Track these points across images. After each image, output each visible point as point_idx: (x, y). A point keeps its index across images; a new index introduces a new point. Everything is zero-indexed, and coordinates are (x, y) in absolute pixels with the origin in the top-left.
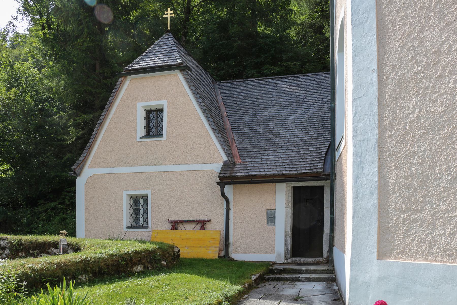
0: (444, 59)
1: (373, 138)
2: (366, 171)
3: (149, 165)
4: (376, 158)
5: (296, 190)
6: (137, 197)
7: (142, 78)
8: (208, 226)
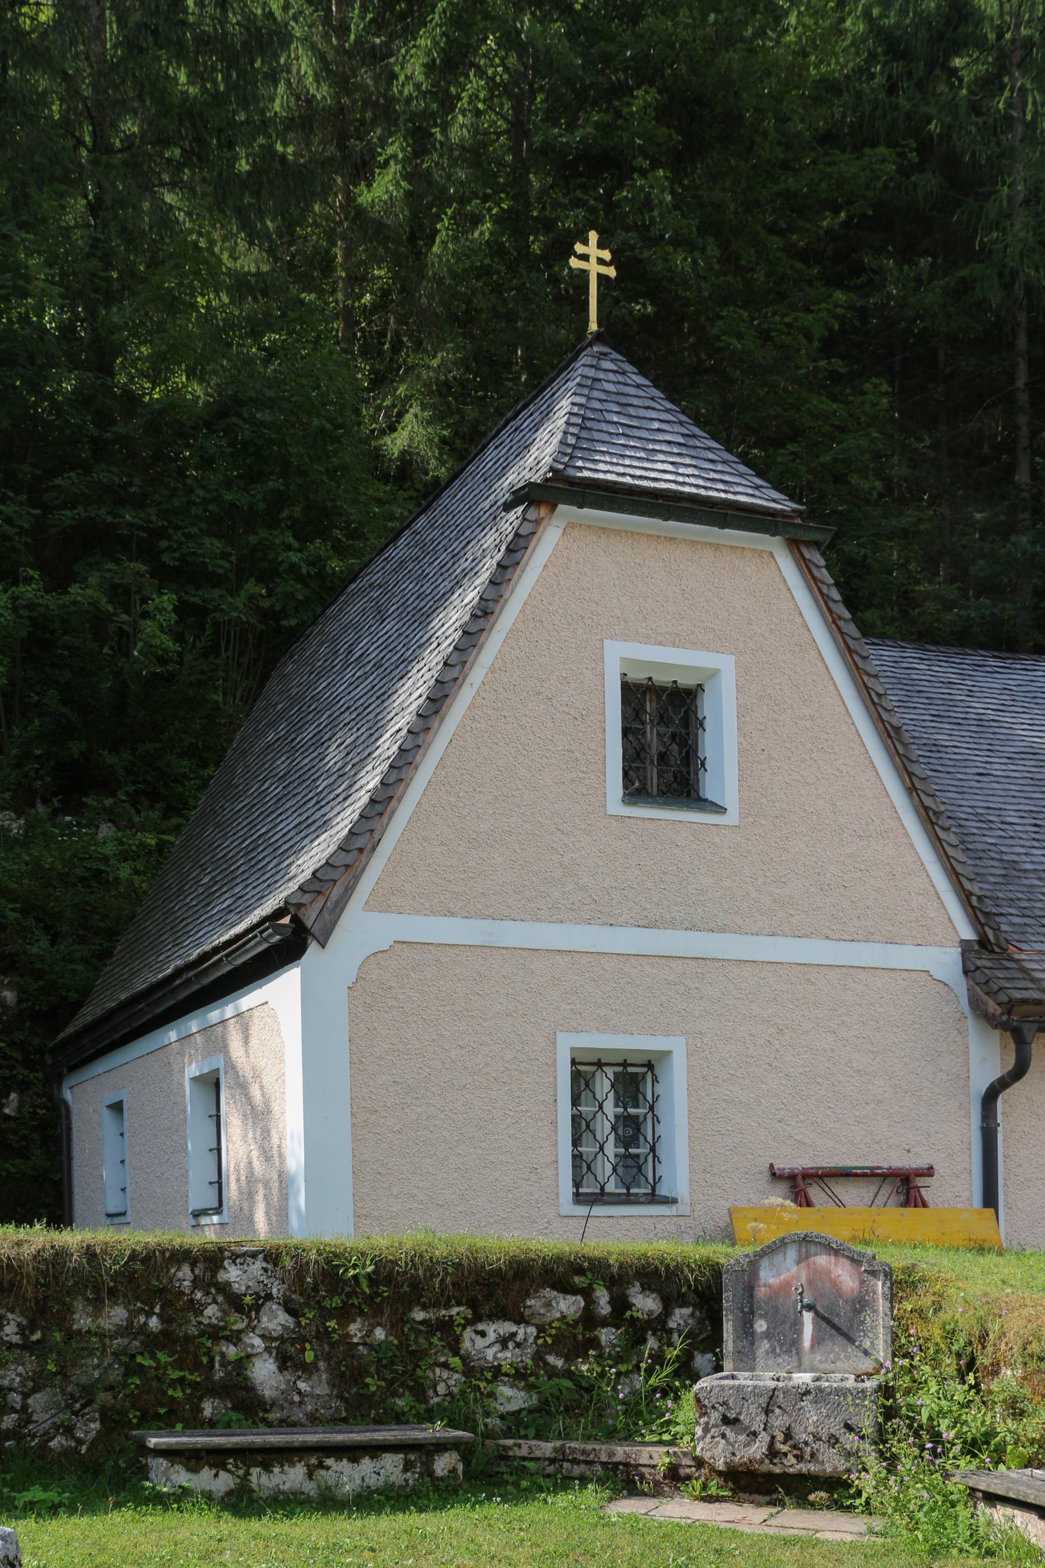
3: (672, 924)
6: (625, 1064)
7: (617, 532)
8: (931, 1190)
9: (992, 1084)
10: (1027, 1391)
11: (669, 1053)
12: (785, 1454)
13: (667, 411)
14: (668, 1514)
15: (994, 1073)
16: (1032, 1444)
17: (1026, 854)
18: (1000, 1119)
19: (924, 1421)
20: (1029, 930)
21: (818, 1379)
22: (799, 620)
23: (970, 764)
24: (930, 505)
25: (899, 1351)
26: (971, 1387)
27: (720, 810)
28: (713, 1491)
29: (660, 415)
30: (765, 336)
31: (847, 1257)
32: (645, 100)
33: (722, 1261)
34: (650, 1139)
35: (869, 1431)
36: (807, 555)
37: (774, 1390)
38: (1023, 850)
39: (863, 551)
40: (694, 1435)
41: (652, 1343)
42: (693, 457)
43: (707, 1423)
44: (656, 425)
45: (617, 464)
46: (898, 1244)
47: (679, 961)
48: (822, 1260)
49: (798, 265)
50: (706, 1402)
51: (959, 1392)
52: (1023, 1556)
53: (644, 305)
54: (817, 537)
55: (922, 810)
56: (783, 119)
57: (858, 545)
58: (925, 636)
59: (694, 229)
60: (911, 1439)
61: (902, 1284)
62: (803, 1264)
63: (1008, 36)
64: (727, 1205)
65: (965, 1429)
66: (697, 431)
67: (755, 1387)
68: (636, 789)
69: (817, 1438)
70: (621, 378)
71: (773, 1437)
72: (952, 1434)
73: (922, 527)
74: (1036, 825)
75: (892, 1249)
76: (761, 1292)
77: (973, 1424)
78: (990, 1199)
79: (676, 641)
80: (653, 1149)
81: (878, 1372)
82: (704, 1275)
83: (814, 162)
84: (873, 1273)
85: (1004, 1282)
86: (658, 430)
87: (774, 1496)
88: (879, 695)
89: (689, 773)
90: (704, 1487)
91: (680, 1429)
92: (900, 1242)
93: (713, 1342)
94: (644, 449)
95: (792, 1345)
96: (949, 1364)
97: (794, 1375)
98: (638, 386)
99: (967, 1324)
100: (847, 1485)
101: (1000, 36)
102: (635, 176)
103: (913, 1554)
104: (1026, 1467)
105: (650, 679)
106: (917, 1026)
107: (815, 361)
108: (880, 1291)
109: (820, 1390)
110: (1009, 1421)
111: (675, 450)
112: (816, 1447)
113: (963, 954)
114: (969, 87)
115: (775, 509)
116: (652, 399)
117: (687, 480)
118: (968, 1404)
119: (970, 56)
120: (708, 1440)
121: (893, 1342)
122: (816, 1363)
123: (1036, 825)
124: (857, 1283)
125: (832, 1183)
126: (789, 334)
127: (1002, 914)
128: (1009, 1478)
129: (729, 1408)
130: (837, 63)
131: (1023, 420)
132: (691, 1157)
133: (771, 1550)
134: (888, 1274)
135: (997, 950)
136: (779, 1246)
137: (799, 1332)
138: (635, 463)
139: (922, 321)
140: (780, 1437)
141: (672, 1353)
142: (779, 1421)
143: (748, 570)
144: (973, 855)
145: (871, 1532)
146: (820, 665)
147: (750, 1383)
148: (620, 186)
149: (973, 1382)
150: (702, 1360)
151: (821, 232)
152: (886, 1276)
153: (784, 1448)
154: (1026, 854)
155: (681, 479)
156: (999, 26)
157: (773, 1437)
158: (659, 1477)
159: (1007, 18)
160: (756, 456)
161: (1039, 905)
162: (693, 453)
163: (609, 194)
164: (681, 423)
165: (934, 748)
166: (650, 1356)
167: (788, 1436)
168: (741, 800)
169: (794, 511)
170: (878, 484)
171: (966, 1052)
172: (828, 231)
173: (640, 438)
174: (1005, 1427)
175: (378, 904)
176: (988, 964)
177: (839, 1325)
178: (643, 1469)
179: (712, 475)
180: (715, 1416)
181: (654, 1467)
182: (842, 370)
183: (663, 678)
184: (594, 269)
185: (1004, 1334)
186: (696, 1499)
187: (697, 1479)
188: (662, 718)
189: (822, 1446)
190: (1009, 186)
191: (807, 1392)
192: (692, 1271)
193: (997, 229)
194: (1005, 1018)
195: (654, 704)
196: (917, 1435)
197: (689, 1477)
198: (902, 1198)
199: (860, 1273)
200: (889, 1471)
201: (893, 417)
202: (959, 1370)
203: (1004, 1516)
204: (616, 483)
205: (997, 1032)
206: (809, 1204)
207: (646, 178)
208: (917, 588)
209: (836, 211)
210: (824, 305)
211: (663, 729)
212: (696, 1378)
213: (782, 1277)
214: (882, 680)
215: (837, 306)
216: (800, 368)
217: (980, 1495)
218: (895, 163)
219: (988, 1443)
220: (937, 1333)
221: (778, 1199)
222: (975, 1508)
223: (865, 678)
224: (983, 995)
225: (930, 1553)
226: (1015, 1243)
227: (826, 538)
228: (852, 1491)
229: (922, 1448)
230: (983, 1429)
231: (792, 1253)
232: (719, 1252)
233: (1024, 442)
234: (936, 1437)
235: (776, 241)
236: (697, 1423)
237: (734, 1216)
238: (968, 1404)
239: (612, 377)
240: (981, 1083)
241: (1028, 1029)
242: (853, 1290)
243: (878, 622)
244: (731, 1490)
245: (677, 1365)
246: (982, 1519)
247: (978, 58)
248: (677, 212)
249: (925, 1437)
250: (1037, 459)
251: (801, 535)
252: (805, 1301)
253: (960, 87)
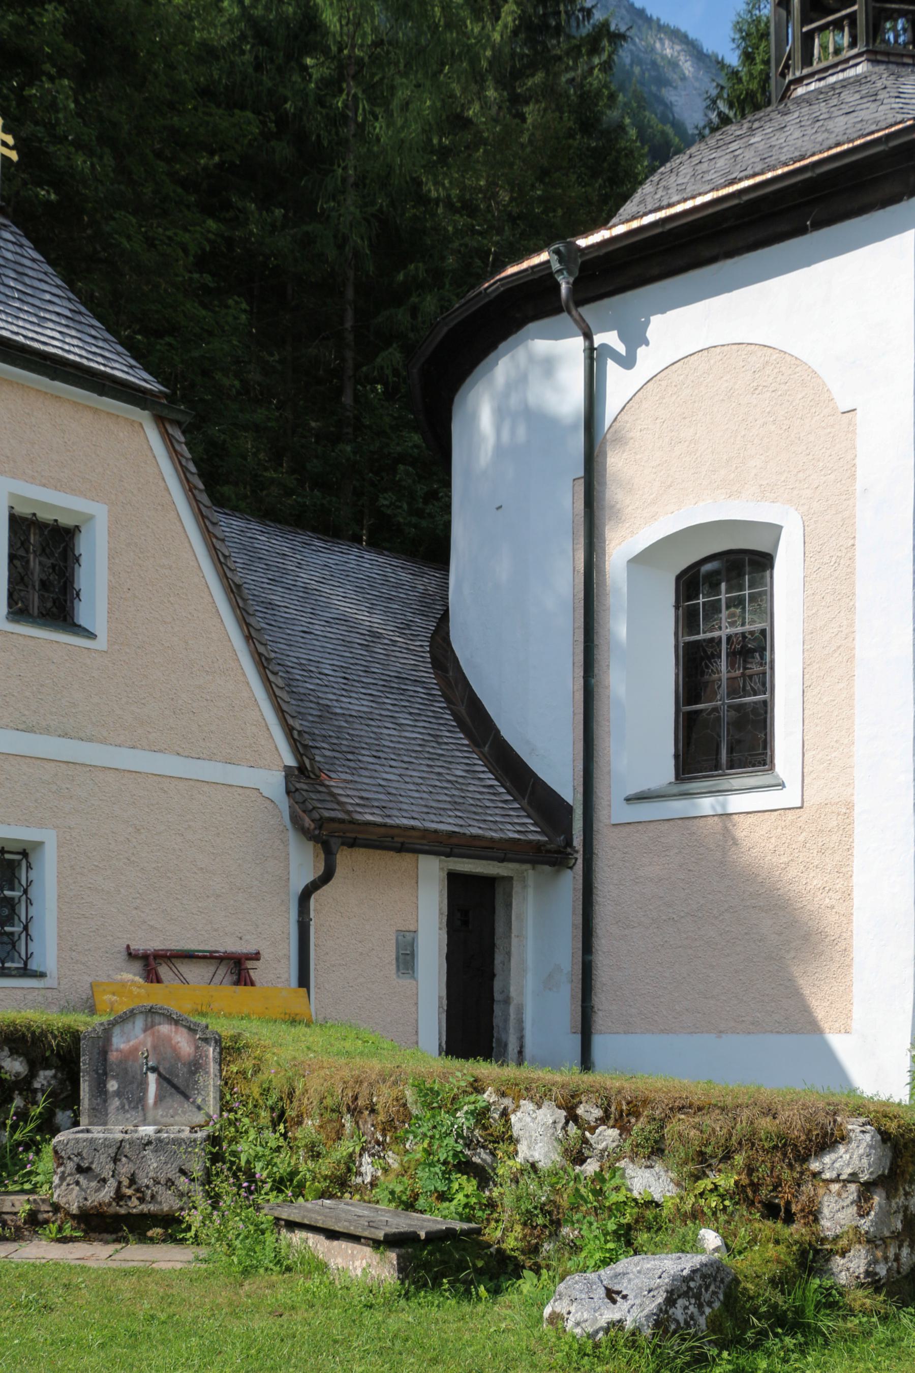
3: (47, 731)
7: (10, 383)
9: (307, 886)
10: (322, 1137)
11: (41, 844)
12: (130, 1197)
13: (58, 286)
14: (26, 1256)
15: (309, 877)
16: (325, 1180)
17: (337, 701)
18: (312, 915)
19: (243, 1163)
20: (337, 762)
21: (159, 1131)
22: (161, 483)
23: (297, 622)
24: (278, 409)
25: (225, 1106)
26: (281, 1135)
27: (91, 636)
28: (67, 1232)
29: (50, 287)
30: (151, 243)
31: (185, 1026)
32: (54, 15)
33: (82, 1028)
34: (23, 919)
35: (198, 1173)
36: (170, 431)
37: (121, 1141)
38: (334, 697)
39: (223, 437)
40: (51, 1183)
41: (18, 1102)
42: (78, 331)
43: (63, 1173)
44: (48, 297)
45: (12, 324)
46: (228, 1016)
47: (53, 764)
48: (165, 1029)
49: (179, 190)
50: (63, 1154)
51: (273, 1139)
52: (313, 1269)
53: (48, 192)
54: (179, 417)
55: (256, 656)
56: (171, 67)
57: (219, 430)
58: (269, 514)
59: (94, 138)
60: (231, 1180)
61: (229, 1050)
62: (148, 1032)
63: (346, 52)
64: (90, 979)
65: (275, 1169)
66: (83, 309)
67: (105, 1139)
68: (19, 610)
69: (157, 1182)
70: (18, 250)
71: (120, 1183)
72: (265, 1174)
73: (269, 424)
74: (345, 678)
75: (223, 1021)
76: (113, 1056)
77: (280, 1166)
78: (304, 980)
79: (58, 485)
80: (26, 928)
81: (207, 1125)
82: (65, 1040)
83: (195, 109)
84: (206, 1040)
85: (309, 1048)
86: (50, 302)
87: (120, 1234)
88: (225, 557)
89: (66, 601)
90: (60, 1229)
91: (40, 1178)
92: (230, 1014)
93: (71, 1100)
94: (36, 315)
95: (139, 1102)
96: (265, 1116)
97: (140, 1128)
98: (34, 260)
99: (279, 1082)
100: (179, 1221)
101: (340, 50)
102: (44, 79)
103: (229, 1275)
104: (320, 1198)
105: (34, 514)
106: (249, 834)
107: (190, 272)
108: (211, 1055)
109: (160, 1140)
110: (309, 1162)
111: (63, 322)
112: (155, 1189)
113: (286, 777)
114: (316, 83)
115: (145, 388)
116: (45, 273)
117: (72, 349)
118: (278, 1149)
119: (318, 59)
120: (64, 1187)
121: (221, 1099)
122: (158, 1117)
123: (345, 678)
124: (193, 1049)
125: (174, 960)
126: (170, 245)
127: (317, 748)
128: (308, 1208)
129: (83, 1159)
130: (216, 33)
131: (349, 354)
132: (59, 937)
133: (113, 1281)
134: (218, 1042)
135: (313, 776)
136: (129, 1016)
137: (145, 1090)
138: (28, 326)
139: (275, 259)
140: (126, 1182)
141: (36, 1111)
142: (125, 1168)
143: (121, 434)
144: (297, 697)
145: (197, 1259)
146: (178, 524)
147: (101, 1135)
148: (31, 85)
149: (283, 1131)
150: (62, 1117)
151: (199, 168)
152: (216, 1043)
153: (129, 1192)
154: (337, 701)
155: (67, 347)
156: (339, 43)
157: (120, 1183)
158: (20, 1223)
159: (345, 38)
160: (139, 341)
161: (345, 742)
162: (78, 327)
163: (21, 87)
164: (69, 299)
165: (269, 606)
166: (15, 1114)
167: (133, 1181)
168: (109, 629)
169: (161, 392)
170: (237, 383)
171: (287, 858)
172: (205, 168)
173: (33, 305)
174: (305, 1167)
176: (305, 787)
177: (178, 1084)
178: (6, 1217)
179: (94, 349)
180: (70, 1166)
181: (15, 1214)
182: (212, 285)
183: (45, 516)
185: (307, 1091)
186: (53, 1240)
187: (53, 1223)
188: (43, 550)
189: (159, 1189)
190: (343, 169)
191: (149, 1143)
192: (55, 1037)
193: (334, 200)
194: (317, 832)
195: (37, 537)
196: (235, 1176)
197: (47, 1222)
198: (235, 977)
199: (195, 1040)
200: (214, 1208)
201: (251, 332)
202: (272, 1121)
203: (300, 1238)
204: (9, 339)
205: (311, 843)
206: (159, 981)
207: (53, 83)
208: (265, 474)
209: (212, 154)
210: (198, 228)
211: (44, 559)
212: (55, 1131)
213: (131, 1043)
214: (227, 543)
215: (209, 231)
216: (177, 275)
217: (283, 1223)
218: (258, 128)
219: (291, 1181)
220: (256, 1092)
221: (132, 976)
222: (279, 1233)
223: (214, 540)
224: (301, 813)
225: (242, 1273)
226: (320, 1017)
227: (187, 420)
228: (183, 1226)
229: (240, 1187)
230: (289, 1169)
231: (140, 1023)
232: (81, 1021)
233: (350, 372)
234: (251, 1176)
235: (162, 166)
236: (55, 1172)
237: (95, 989)
238: (278, 1149)
239: (10, 247)
240: (299, 882)
241: (334, 842)
242: (189, 1055)
243: (233, 497)
244: (83, 1231)
245: (39, 1122)
246: (283, 1242)
247: (323, 63)
248: (80, 120)
249: (243, 1178)
250: (359, 387)
251: (165, 413)
252: (150, 1064)
253: (310, 81)
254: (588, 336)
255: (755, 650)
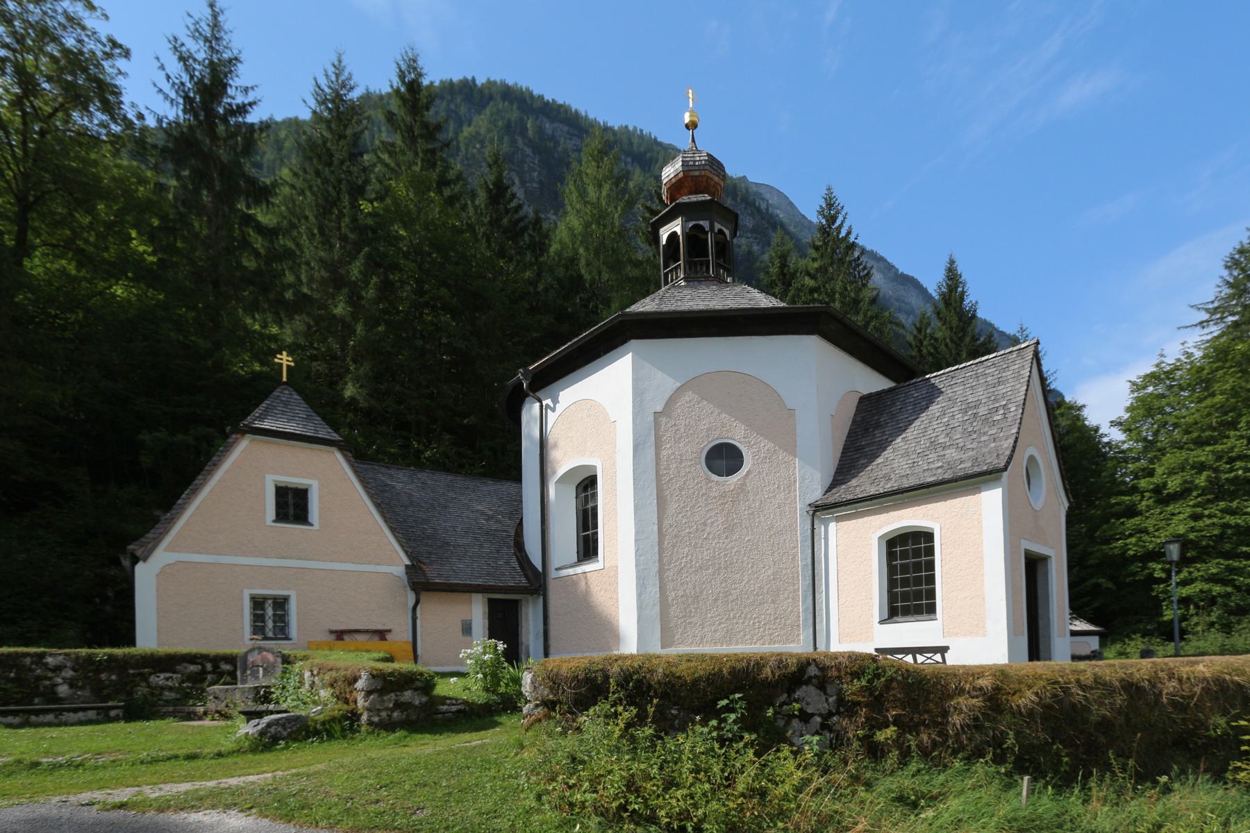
0: (708, 529)
1: (655, 568)
2: (649, 589)
3: (291, 558)
4: (657, 582)
5: (491, 601)
8: (388, 636)
136: (252, 650)
175: (170, 549)
184: (285, 363)
254: (540, 401)
255: (595, 509)
